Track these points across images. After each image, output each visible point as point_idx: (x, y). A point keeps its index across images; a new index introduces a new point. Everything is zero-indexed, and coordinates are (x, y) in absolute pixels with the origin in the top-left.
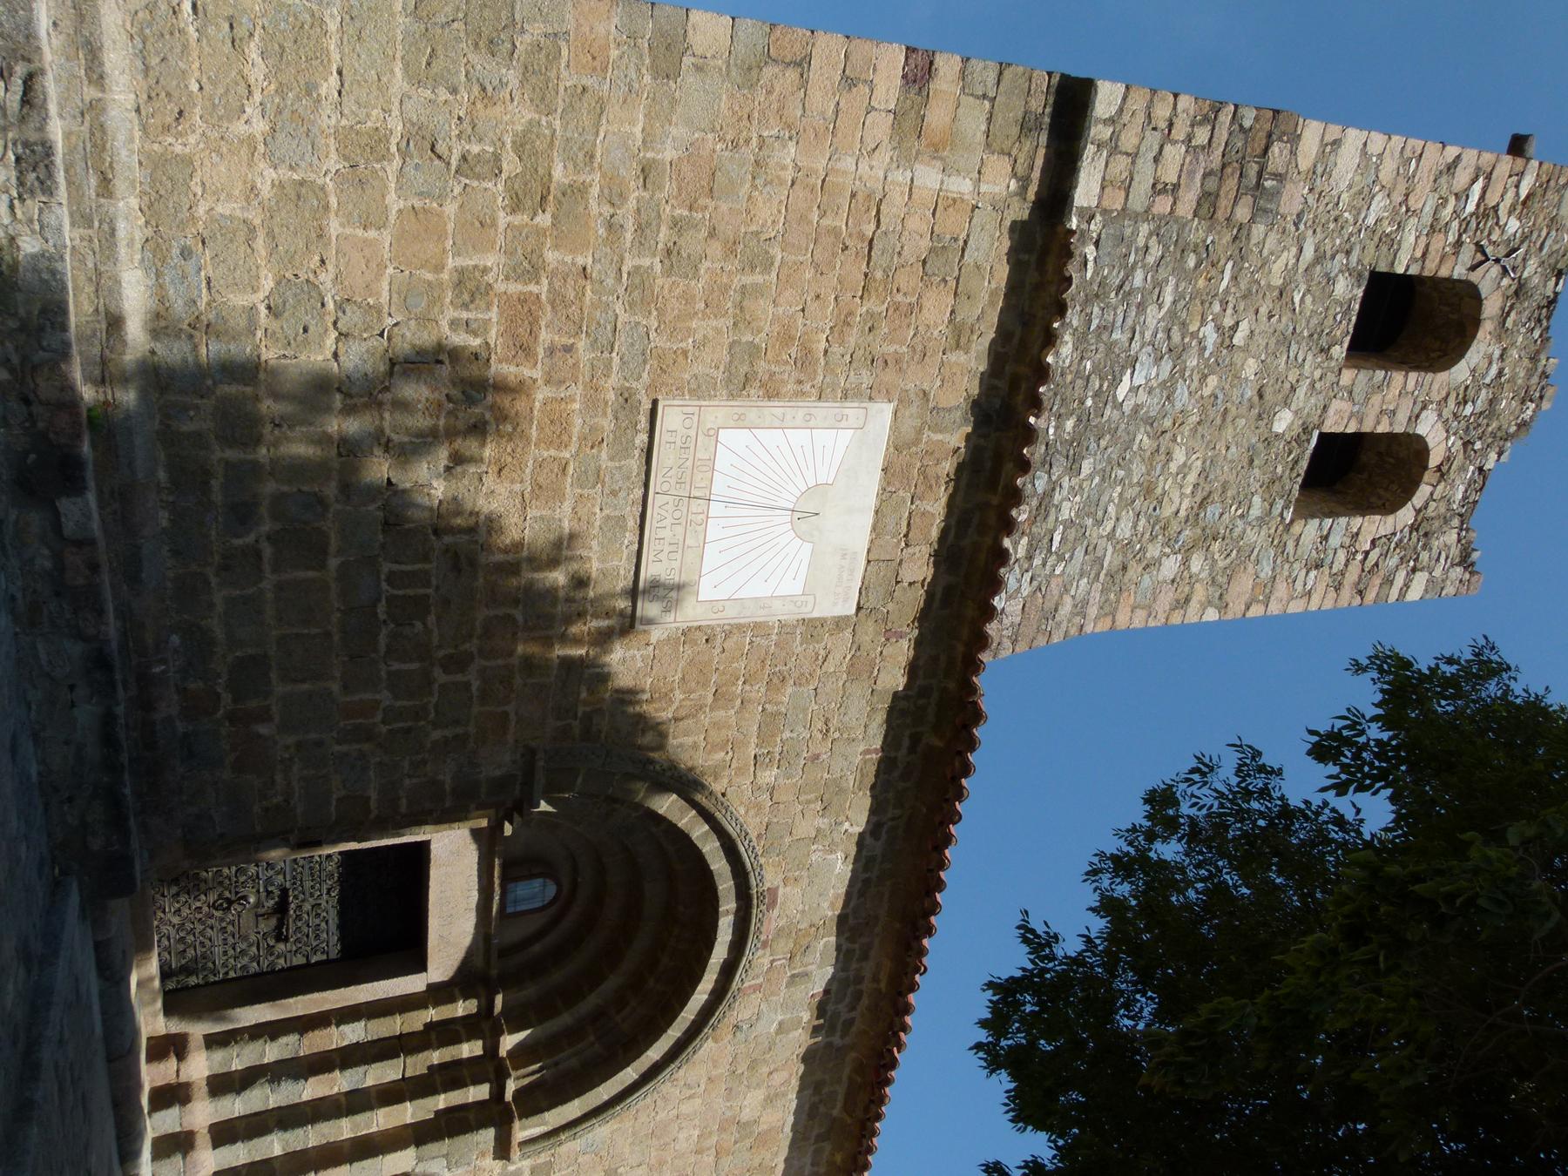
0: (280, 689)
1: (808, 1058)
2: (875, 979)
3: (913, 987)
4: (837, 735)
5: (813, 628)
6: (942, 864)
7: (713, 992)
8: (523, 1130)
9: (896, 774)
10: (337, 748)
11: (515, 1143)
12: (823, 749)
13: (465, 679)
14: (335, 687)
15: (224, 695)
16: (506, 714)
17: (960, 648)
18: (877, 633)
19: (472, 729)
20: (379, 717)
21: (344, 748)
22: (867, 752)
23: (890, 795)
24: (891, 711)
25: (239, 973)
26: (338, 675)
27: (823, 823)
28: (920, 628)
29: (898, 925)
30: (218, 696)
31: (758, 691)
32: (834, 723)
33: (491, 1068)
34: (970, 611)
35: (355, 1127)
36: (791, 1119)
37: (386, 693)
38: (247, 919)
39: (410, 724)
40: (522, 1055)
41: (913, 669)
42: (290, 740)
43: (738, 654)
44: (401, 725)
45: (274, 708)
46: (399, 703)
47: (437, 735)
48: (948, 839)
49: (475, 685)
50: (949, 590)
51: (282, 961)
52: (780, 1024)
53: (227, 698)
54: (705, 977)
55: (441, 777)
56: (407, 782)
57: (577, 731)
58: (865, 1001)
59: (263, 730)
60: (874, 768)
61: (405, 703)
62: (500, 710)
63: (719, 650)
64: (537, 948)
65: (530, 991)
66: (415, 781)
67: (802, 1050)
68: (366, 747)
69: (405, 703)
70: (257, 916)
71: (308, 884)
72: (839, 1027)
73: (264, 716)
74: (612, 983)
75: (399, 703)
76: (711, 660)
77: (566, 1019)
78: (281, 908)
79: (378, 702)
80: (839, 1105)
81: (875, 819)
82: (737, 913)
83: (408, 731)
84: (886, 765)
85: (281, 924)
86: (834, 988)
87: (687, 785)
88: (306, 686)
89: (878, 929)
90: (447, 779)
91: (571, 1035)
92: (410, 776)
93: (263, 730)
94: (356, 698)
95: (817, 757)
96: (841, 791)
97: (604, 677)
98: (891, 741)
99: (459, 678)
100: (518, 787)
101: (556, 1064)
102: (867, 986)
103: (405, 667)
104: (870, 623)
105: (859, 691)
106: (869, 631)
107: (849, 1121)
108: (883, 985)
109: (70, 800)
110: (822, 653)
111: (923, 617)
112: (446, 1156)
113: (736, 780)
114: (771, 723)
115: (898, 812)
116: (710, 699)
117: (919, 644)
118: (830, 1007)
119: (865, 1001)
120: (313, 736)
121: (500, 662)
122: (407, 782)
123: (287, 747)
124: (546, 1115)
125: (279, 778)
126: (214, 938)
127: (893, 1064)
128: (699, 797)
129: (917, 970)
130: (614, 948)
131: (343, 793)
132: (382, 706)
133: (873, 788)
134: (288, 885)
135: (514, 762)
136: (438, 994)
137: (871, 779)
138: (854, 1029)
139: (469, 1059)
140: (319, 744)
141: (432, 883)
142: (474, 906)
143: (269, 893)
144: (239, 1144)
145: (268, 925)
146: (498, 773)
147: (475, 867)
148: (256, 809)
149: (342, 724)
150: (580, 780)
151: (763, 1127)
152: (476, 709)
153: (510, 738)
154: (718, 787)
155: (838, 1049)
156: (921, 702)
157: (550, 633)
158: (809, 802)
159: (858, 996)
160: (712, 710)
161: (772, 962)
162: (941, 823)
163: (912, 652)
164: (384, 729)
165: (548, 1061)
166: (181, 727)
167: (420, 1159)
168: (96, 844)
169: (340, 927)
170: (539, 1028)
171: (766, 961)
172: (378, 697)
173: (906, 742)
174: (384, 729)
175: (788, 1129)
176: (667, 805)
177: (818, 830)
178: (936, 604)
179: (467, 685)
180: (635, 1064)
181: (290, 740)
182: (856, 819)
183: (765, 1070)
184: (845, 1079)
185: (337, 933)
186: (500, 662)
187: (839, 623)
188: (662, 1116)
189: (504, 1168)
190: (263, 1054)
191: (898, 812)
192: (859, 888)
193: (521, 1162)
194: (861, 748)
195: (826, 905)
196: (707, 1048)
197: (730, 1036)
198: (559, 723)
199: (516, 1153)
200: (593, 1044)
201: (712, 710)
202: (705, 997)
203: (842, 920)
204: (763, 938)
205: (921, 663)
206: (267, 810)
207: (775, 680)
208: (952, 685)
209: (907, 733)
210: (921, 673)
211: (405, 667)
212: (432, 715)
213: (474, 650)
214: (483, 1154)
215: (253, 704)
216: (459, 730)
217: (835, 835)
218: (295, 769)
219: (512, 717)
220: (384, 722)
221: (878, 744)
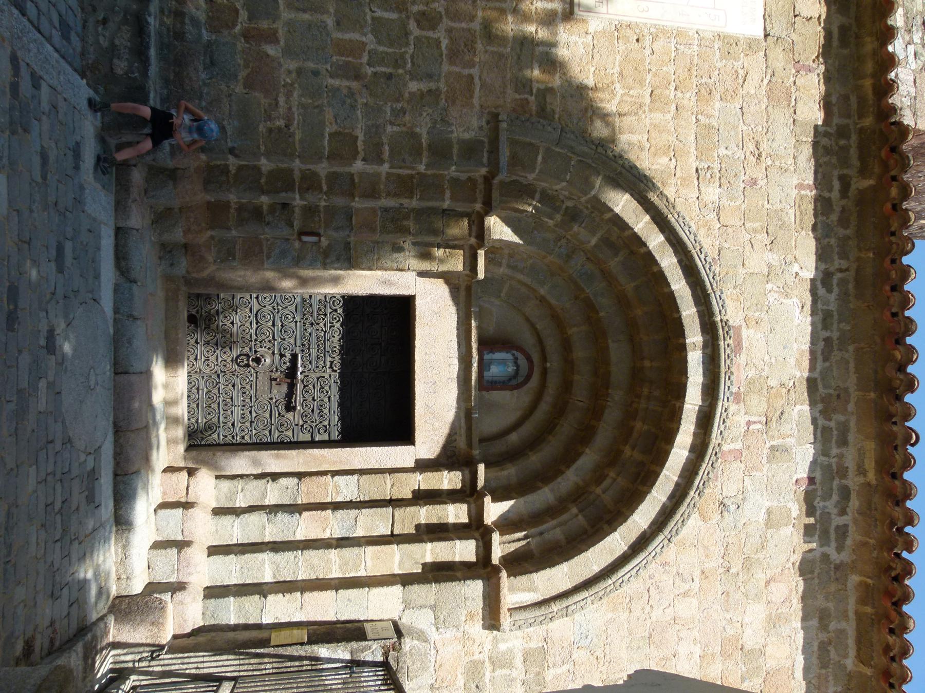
0: (286, 15)
1: (806, 568)
2: (861, 471)
3: (908, 463)
4: (769, 162)
5: (729, 44)
6: (906, 301)
7: (692, 449)
8: (515, 592)
9: (834, 217)
10: (331, 81)
11: (504, 612)
12: (759, 174)
13: (435, 36)
14: (330, 22)
15: (241, 12)
16: (471, 77)
17: (868, 83)
18: (787, 62)
19: (442, 86)
20: (365, 59)
21: (336, 82)
22: (800, 187)
23: (833, 241)
24: (815, 145)
25: (254, 440)
26: (332, 10)
27: (774, 258)
28: (825, 63)
29: (872, 395)
30: (237, 11)
31: (688, 99)
32: (764, 147)
33: (475, 528)
34: (869, 45)
35: (344, 564)
36: (800, 660)
37: (370, 36)
38: (263, 380)
39: (389, 70)
40: (506, 525)
41: (827, 104)
42: (293, 65)
43: (666, 58)
44: (383, 69)
45: (280, 31)
46: (381, 49)
47: (413, 86)
48: (905, 273)
49: (445, 43)
50: (843, 30)
51: (290, 433)
52: (769, 512)
53: (243, 15)
54: (683, 428)
55: (418, 130)
56: (389, 129)
57: (534, 107)
58: (854, 503)
59: (271, 50)
60: (811, 207)
61: (386, 49)
62: (466, 72)
63: (649, 51)
64: (514, 437)
65: (510, 472)
66: (395, 129)
67: (797, 558)
68: (355, 85)
69: (386, 49)
70: (272, 379)
71: (314, 352)
72: (833, 536)
73: (272, 37)
74: (588, 459)
75: (381, 49)
76: (643, 60)
77: (544, 496)
78: (291, 373)
79: (364, 44)
80: (852, 652)
81: (823, 266)
82: (705, 347)
83: (389, 77)
84: (822, 205)
85: (290, 394)
86: (818, 475)
87: (638, 184)
88: (306, 16)
89: (851, 407)
90: (423, 132)
91: (551, 512)
92: (392, 124)
93: (271, 50)
94: (347, 36)
95: (754, 182)
96: (783, 226)
97: (552, 64)
98: (822, 179)
99: (430, 34)
100: (485, 155)
101: (541, 534)
102: (853, 481)
103: (386, 15)
104: (779, 50)
105: (781, 117)
106: (779, 59)
107: (868, 671)
108: (871, 476)
109: (105, 22)
110: (741, 72)
111: (826, 51)
112: (433, 607)
113: (683, 192)
114: (706, 135)
115: (844, 264)
116: (648, 100)
117: (828, 78)
118: (819, 503)
119: (854, 503)
120: (311, 65)
121: (464, 25)
122: (389, 129)
123: (289, 72)
124: (535, 576)
125: (282, 100)
126: (235, 397)
127: (908, 569)
128: (653, 197)
129: (907, 440)
130: (584, 424)
131: (334, 128)
132: (368, 48)
133: (814, 228)
134: (298, 350)
135: (481, 128)
136: (422, 466)
137: (810, 220)
138: (849, 542)
139: (455, 525)
140: (316, 73)
141: (418, 343)
142: (455, 376)
143: (282, 355)
144: (232, 556)
145: (279, 392)
146: (467, 136)
147: (455, 332)
148: (261, 128)
149: (334, 59)
150: (540, 158)
151: (771, 664)
152: (446, 67)
153: (476, 101)
154: (670, 192)
155: (837, 567)
156: (842, 142)
157: (504, 5)
158: (755, 231)
159: (845, 493)
160: (651, 110)
161: (749, 423)
162: (893, 261)
163: (823, 88)
164: (369, 71)
165: (533, 531)
166: (206, 36)
167: (407, 605)
168: (120, 67)
169: (341, 405)
170: (522, 500)
171: (742, 419)
172: (364, 39)
173: (837, 185)
174: (369, 71)
175: (799, 674)
176: (622, 203)
177: (770, 266)
178: (835, 43)
179: (438, 43)
180: (622, 529)
181: (293, 65)
182: (806, 266)
183: (761, 577)
184: (851, 614)
185: (338, 411)
186: (464, 25)
187: (751, 44)
188: (657, 614)
189: (495, 641)
190: (264, 494)
191: (844, 264)
192: (823, 348)
193: (514, 639)
194: (795, 182)
195: (792, 361)
196: (692, 525)
197: (717, 516)
198: (517, 97)
199: (506, 620)
200: (577, 515)
201: (651, 110)
202: (686, 453)
203: (812, 384)
204: (734, 389)
205: (834, 99)
206: (270, 131)
207: (703, 91)
208: (868, 121)
209: (836, 173)
210: (835, 110)
211: (386, 15)
212: (409, 65)
213: (441, 9)
214: (471, 616)
215: (264, 25)
216: (433, 86)
217: (787, 275)
218: (295, 94)
219: (477, 80)
220: (369, 64)
221: (810, 180)
